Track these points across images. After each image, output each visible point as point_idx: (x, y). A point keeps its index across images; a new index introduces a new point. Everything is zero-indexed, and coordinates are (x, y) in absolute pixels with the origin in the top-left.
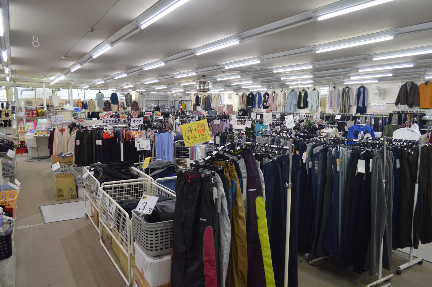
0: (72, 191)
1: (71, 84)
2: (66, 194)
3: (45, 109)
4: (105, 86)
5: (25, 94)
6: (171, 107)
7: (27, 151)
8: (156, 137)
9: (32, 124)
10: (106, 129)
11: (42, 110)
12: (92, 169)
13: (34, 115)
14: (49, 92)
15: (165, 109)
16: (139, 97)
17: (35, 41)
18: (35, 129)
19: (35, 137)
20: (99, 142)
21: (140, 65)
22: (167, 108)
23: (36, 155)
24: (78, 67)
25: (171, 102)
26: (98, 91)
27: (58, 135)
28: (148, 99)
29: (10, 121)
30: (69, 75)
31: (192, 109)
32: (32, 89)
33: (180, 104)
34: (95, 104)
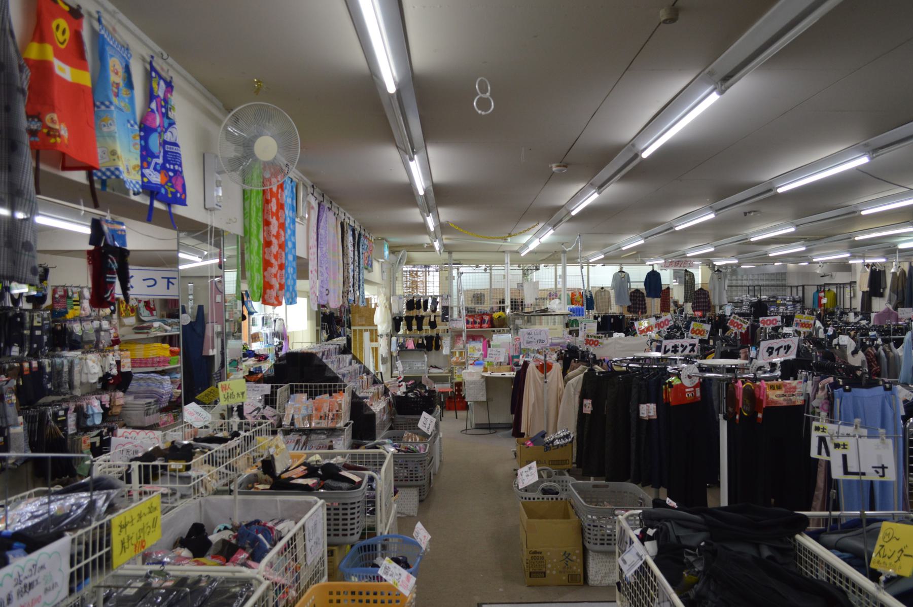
0: (570, 563)
1: (564, 252)
2: (552, 568)
3: (508, 311)
4: (638, 255)
5: (472, 278)
6: (795, 302)
7: (466, 407)
8: (838, 401)
9: (479, 345)
10: (678, 376)
11: (501, 313)
12: (651, 532)
13: (485, 325)
14: (515, 274)
15: (778, 305)
16: (712, 278)
17: (480, 95)
18: (485, 356)
19: (483, 377)
20: (648, 410)
21: (767, 176)
22: (782, 305)
23: (484, 420)
24: (592, 198)
25: (794, 290)
26: (616, 268)
27: (535, 381)
28: (734, 283)
29: (438, 338)
30: (562, 226)
31: (857, 304)
32: (485, 270)
33: (822, 294)
34: (609, 298)
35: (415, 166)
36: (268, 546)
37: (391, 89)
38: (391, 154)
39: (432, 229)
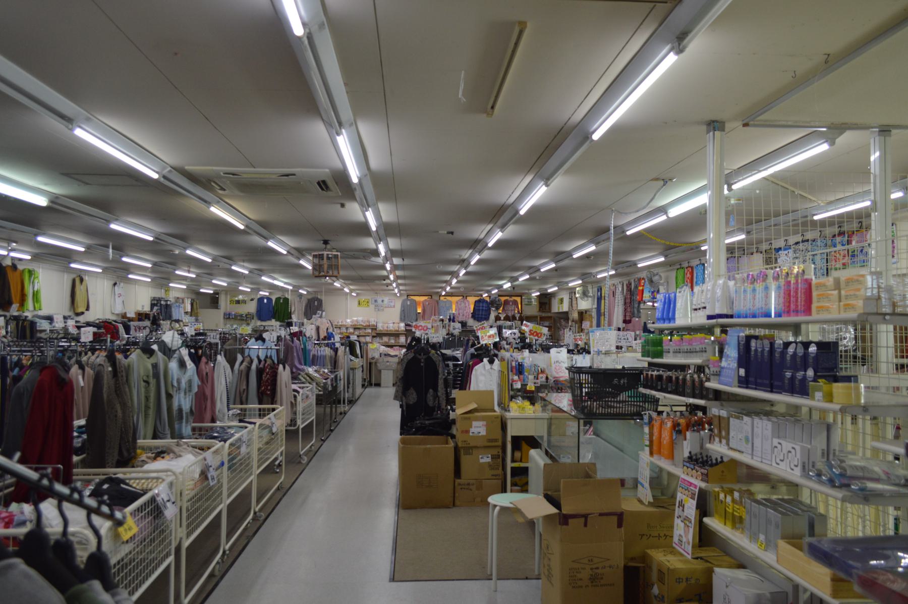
35: (343, 142)
36: (498, 508)
37: (298, 30)
38: (319, 129)
39: (374, 228)
